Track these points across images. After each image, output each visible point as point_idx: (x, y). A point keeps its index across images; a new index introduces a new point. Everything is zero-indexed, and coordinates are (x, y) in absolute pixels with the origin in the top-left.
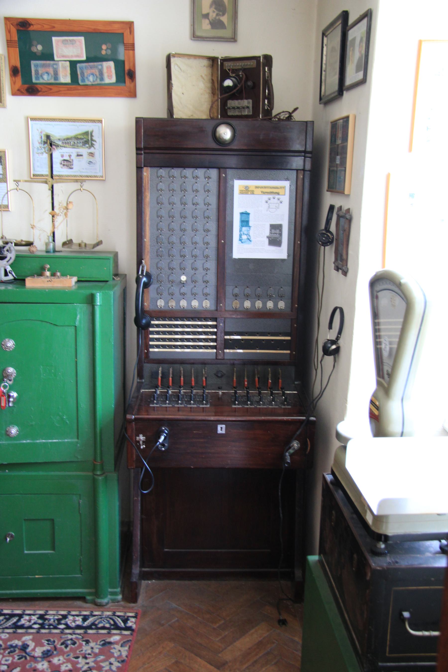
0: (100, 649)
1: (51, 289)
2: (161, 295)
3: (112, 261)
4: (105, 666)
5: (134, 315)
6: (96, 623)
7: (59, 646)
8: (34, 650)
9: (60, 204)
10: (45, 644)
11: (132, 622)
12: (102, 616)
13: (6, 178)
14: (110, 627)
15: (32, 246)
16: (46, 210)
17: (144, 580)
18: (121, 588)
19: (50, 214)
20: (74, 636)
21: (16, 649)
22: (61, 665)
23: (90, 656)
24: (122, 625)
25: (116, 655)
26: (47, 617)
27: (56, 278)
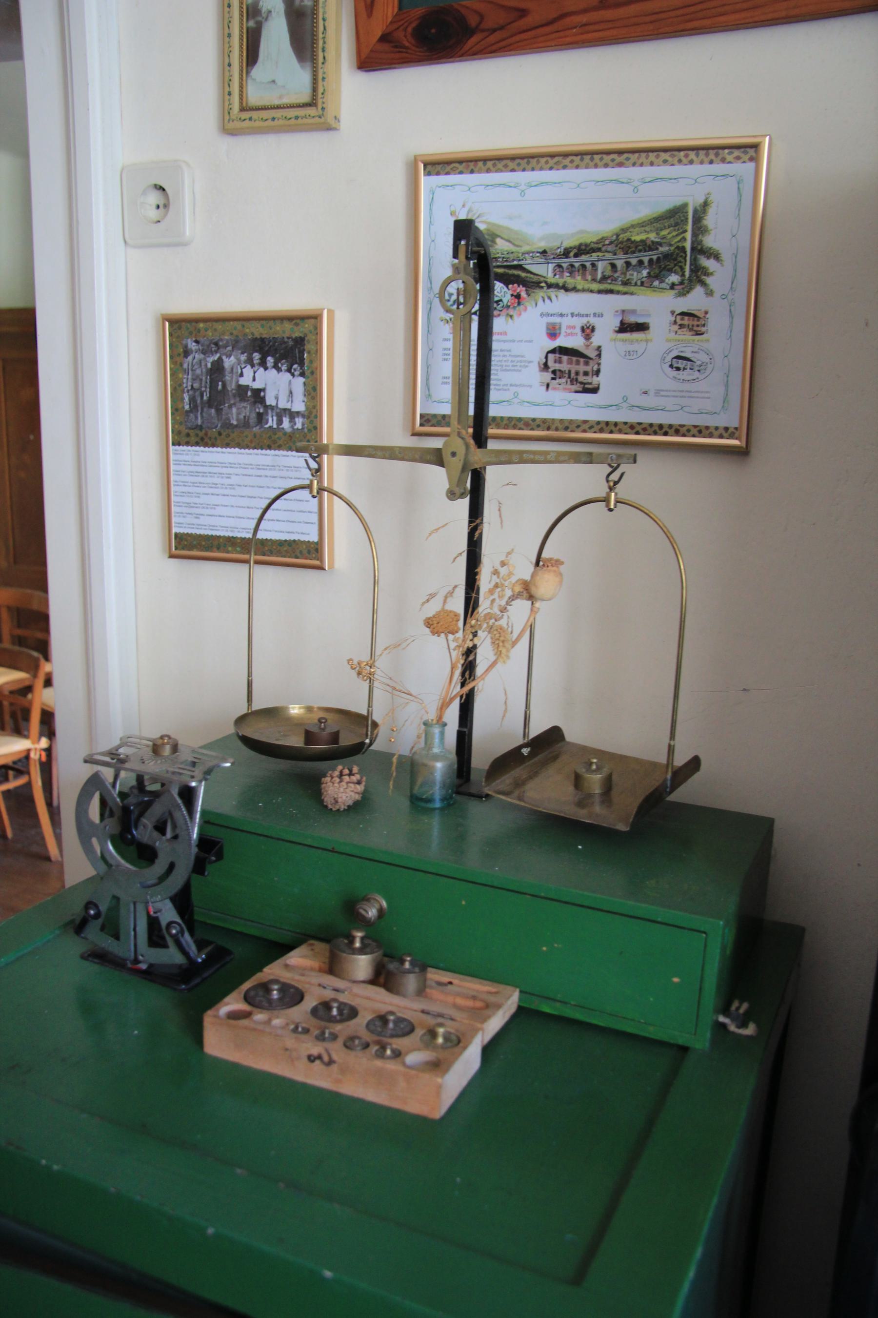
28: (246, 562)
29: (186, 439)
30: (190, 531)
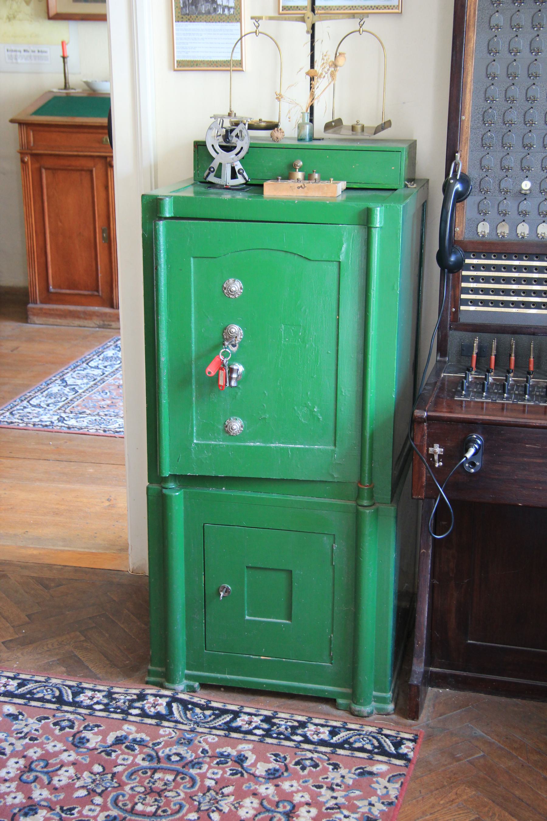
0: (354, 780)
1: (304, 199)
2: (485, 214)
3: (404, 155)
4: (363, 805)
5: (437, 248)
6: (351, 740)
7: (291, 766)
8: (254, 765)
9: (325, 58)
10: (272, 759)
11: (408, 747)
12: (362, 733)
13: (240, 14)
14: (373, 750)
15: (276, 129)
16: (301, 69)
17: (432, 687)
18: (393, 693)
19: (307, 74)
20: (315, 755)
21: (229, 760)
22: (295, 794)
23: (339, 788)
24: (392, 750)
25: (379, 792)
26: (275, 721)
27: (313, 183)
28: (230, 71)
29: (181, 20)
30: (183, 59)
